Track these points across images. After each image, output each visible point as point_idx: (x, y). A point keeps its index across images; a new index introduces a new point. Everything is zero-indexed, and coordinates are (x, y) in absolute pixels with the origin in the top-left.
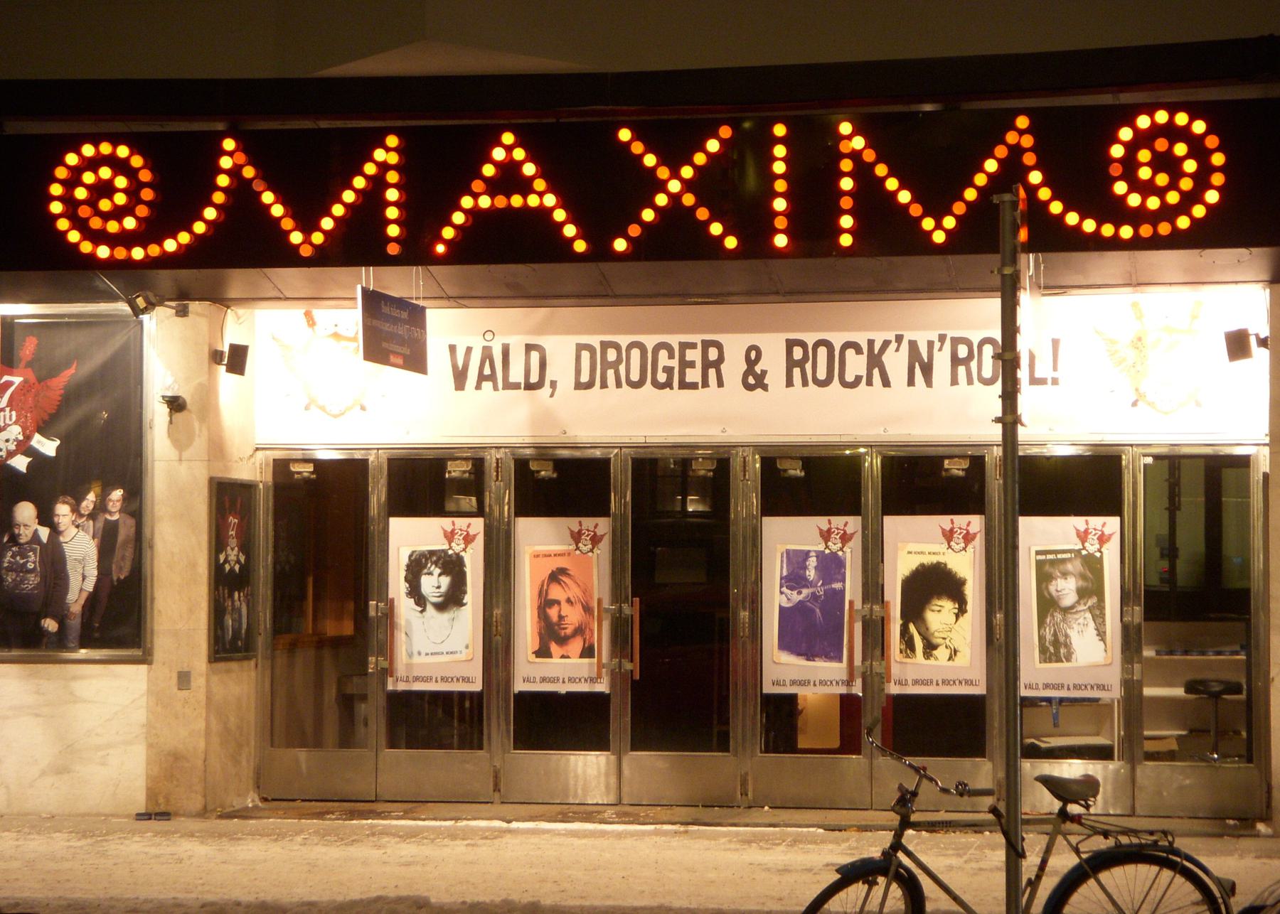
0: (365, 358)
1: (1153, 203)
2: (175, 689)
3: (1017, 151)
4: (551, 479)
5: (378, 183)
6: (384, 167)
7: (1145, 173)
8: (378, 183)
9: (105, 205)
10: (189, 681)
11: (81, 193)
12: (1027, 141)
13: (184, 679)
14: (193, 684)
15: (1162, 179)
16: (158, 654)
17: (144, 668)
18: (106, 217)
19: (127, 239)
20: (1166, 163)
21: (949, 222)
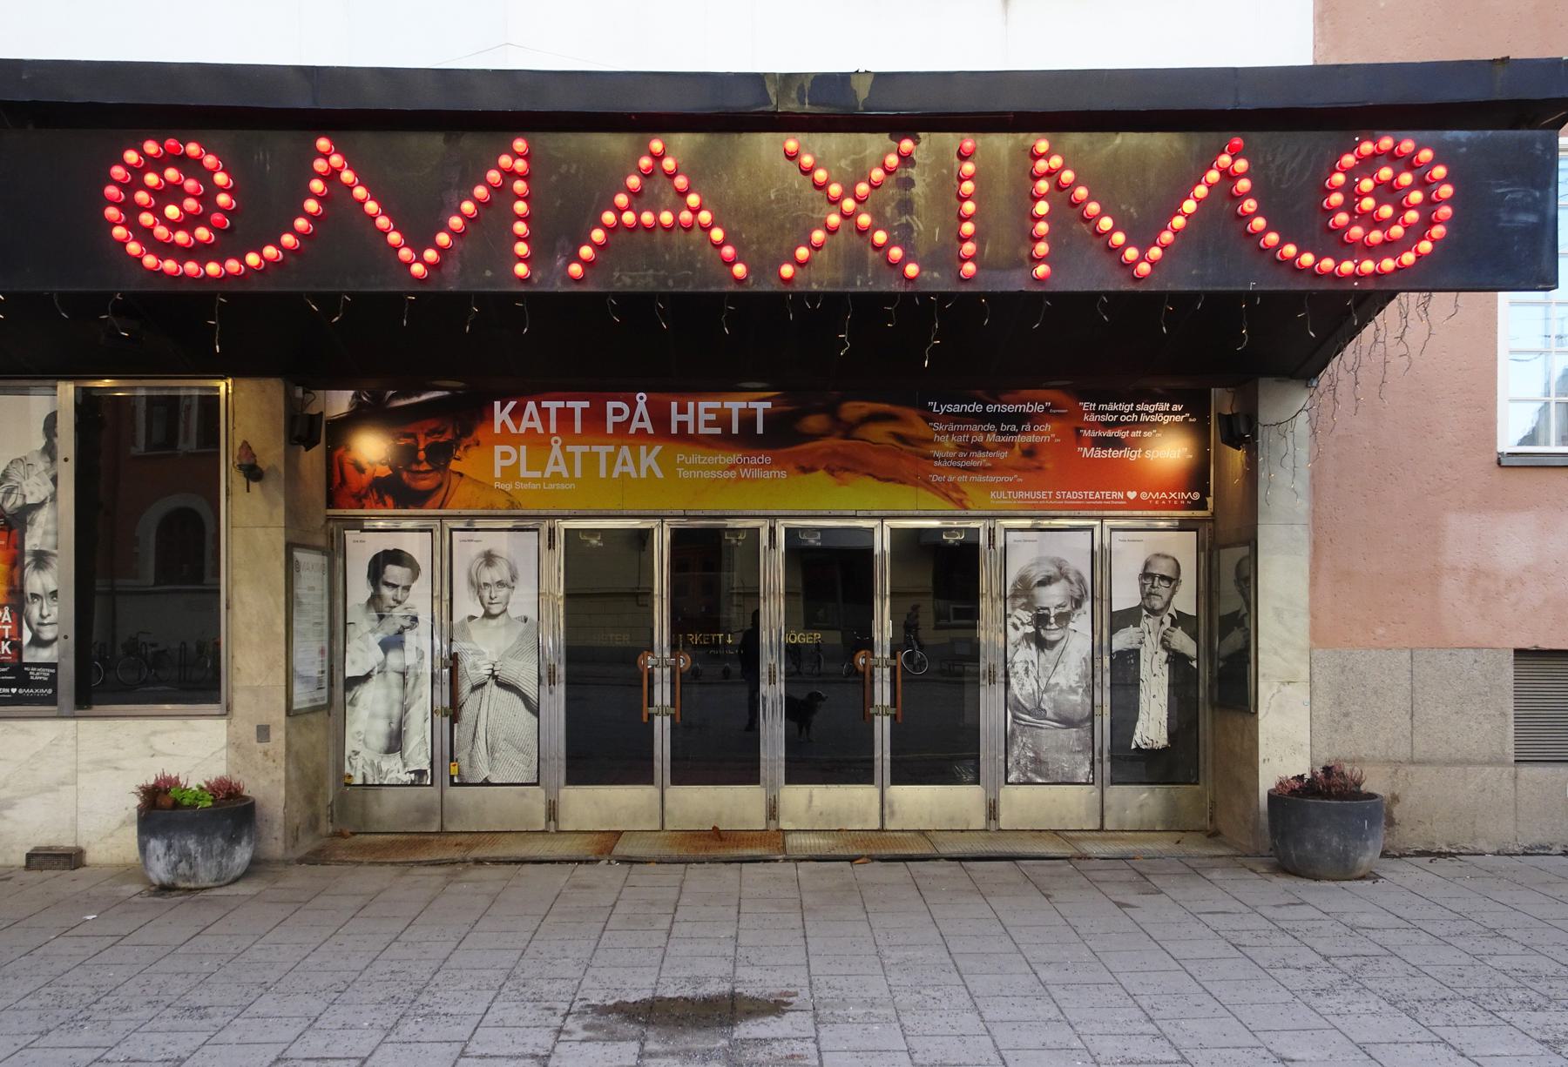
0: (1547, 281)
1: (1376, 236)
2: (254, 742)
3: (332, 176)
4: (598, 548)
5: (502, 193)
6: (509, 174)
7: (1368, 203)
8: (502, 193)
9: (172, 211)
10: (268, 735)
11: (142, 197)
12: (336, 160)
13: (263, 732)
14: (272, 737)
15: (1387, 211)
16: (238, 709)
17: (223, 722)
18: (173, 226)
19: (199, 252)
20: (1387, 191)
21: (1155, 252)
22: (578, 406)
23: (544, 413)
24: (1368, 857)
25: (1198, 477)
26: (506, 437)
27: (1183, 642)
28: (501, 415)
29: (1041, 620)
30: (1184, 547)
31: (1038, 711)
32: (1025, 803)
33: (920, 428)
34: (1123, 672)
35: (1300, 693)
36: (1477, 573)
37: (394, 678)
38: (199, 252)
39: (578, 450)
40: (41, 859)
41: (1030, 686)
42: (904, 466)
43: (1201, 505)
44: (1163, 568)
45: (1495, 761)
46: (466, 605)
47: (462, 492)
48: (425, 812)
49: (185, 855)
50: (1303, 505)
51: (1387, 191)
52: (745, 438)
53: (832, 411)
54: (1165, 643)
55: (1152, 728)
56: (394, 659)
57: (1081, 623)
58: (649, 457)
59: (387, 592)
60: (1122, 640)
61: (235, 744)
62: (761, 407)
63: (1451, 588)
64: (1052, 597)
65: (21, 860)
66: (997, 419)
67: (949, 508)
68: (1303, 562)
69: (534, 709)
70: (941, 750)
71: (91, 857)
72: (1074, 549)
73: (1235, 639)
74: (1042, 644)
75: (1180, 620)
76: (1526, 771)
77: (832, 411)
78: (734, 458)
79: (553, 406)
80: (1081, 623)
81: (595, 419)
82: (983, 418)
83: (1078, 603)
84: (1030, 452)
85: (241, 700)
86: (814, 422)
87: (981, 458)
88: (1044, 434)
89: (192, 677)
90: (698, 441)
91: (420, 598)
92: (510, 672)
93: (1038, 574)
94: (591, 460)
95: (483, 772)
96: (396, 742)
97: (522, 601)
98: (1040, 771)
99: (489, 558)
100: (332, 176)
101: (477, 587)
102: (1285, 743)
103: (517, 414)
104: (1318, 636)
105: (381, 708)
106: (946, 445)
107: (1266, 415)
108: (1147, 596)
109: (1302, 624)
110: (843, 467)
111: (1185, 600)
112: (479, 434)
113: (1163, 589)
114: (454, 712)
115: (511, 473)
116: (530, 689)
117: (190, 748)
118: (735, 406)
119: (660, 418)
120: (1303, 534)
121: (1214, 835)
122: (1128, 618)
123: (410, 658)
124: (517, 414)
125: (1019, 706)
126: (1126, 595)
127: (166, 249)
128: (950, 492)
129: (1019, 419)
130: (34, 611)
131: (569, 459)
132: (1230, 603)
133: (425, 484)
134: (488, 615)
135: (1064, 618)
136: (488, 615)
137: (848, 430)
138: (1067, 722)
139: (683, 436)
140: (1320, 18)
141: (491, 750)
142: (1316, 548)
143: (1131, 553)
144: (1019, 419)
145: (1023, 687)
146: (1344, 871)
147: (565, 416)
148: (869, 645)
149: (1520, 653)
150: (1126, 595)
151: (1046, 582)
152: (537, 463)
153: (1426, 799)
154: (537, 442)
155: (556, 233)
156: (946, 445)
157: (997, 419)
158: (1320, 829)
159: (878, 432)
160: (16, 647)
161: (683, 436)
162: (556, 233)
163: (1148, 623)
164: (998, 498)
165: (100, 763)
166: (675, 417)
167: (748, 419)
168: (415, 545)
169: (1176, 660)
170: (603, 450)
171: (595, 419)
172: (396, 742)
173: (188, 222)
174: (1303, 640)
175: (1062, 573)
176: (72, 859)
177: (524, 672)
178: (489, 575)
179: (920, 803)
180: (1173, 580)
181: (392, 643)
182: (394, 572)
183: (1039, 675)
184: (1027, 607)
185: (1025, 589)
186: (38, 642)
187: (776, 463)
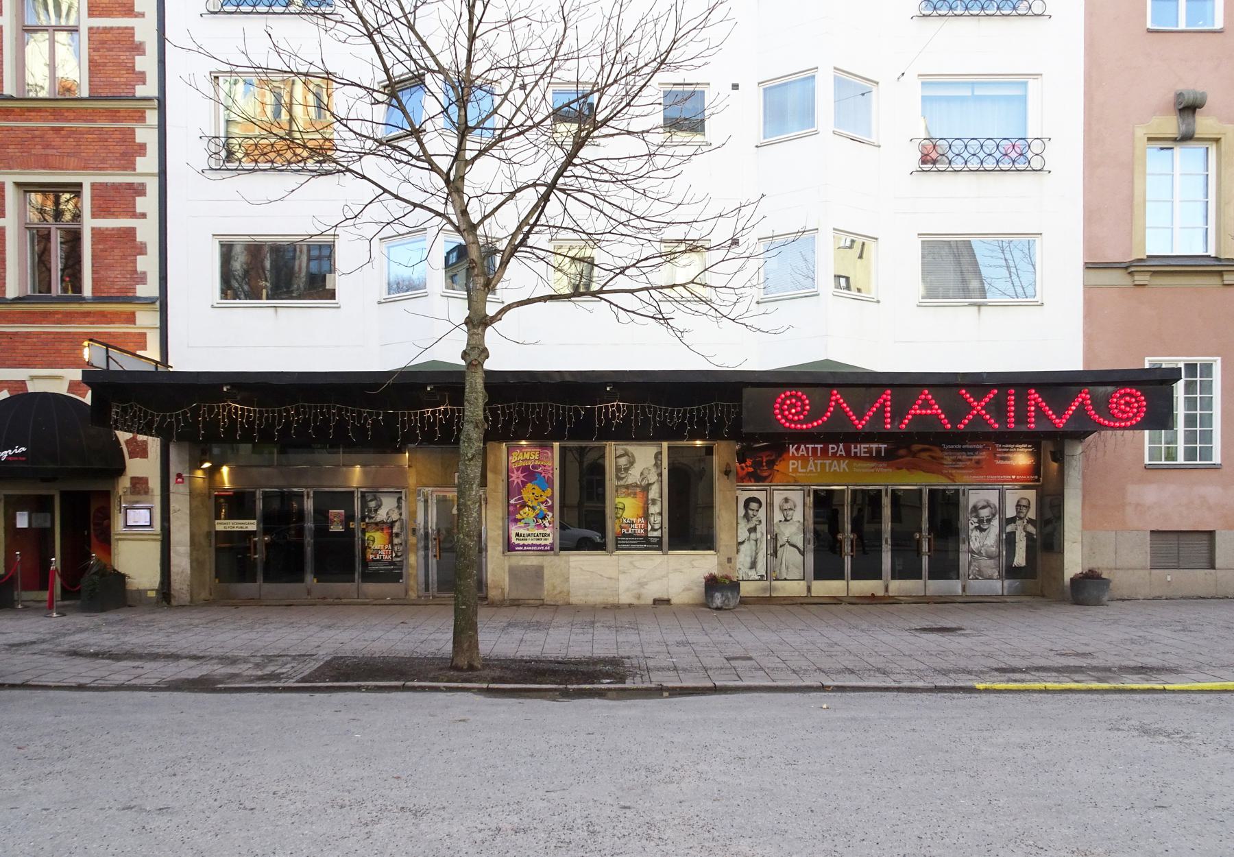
6: (886, 400)
8: (884, 406)
18: (794, 415)
19: (799, 421)
20: (1127, 404)
22: (819, 446)
23: (807, 449)
24: (1105, 598)
25: (1036, 469)
26: (794, 457)
27: (1031, 529)
28: (792, 450)
29: (981, 521)
30: (1031, 495)
31: (980, 553)
32: (978, 587)
33: (938, 453)
34: (1009, 541)
35: (1078, 547)
36: (1138, 505)
37: (753, 543)
38: (799, 421)
39: (819, 462)
40: (657, 602)
41: (977, 545)
42: (934, 466)
43: (1038, 480)
44: (1024, 503)
45: (1143, 568)
46: (778, 516)
47: (778, 477)
48: (764, 590)
49: (728, 598)
50: (1080, 483)
51: (1127, 404)
52: (877, 458)
53: (908, 448)
54: (1024, 529)
55: (1020, 559)
56: (753, 536)
57: (995, 522)
58: (844, 464)
59: (751, 512)
60: (1009, 529)
61: (720, 564)
62: (883, 446)
63: (1129, 510)
64: (985, 513)
65: (650, 601)
66: (966, 450)
67: (949, 482)
68: (1079, 501)
69: (803, 553)
70: (946, 568)
71: (673, 601)
72: (993, 496)
73: (1049, 529)
74: (982, 530)
75: (1030, 521)
76: (1154, 571)
77: (908, 448)
78: (873, 464)
79: (810, 446)
80: (995, 522)
81: (825, 451)
82: (961, 450)
83: (994, 515)
84: (978, 462)
85: (722, 549)
86: (902, 452)
87: (961, 464)
88: (983, 455)
89: (706, 542)
90: (861, 458)
91: (762, 514)
92: (793, 541)
93: (980, 505)
94: (823, 465)
95: (784, 576)
96: (753, 565)
97: (798, 516)
98: (980, 575)
99: (786, 500)
100: (837, 400)
101: (782, 510)
102: (1074, 562)
103: (798, 449)
104: (1084, 527)
105: (749, 553)
106: (948, 459)
107: (1067, 452)
108: (1018, 512)
109: (1079, 523)
110: (912, 467)
111: (1032, 514)
112: (785, 456)
113: (1024, 510)
114: (775, 553)
115: (795, 470)
116: (801, 545)
117: (703, 564)
118: (874, 446)
119: (848, 451)
120: (1079, 492)
121: (1043, 596)
122: (1012, 520)
123: (759, 535)
124: (798, 449)
125: (973, 552)
126: (1010, 512)
127: (792, 421)
128: (950, 477)
129: (974, 450)
130: (652, 519)
131: (816, 465)
132: (1048, 514)
133: (765, 474)
134: (786, 520)
135: (989, 521)
136: (786, 520)
137: (914, 454)
138: (990, 557)
139: (856, 457)
140: (1085, 317)
141: (787, 568)
142: (1084, 496)
143: (1012, 498)
144: (974, 450)
145: (974, 545)
146: (1098, 603)
147: (814, 450)
148: (920, 531)
149: (1152, 532)
150: (1010, 512)
151: (984, 507)
152: (804, 466)
153: (1120, 581)
154: (805, 459)
155: (898, 415)
156: (948, 459)
157: (966, 450)
158: (1088, 590)
159: (925, 455)
160: (646, 531)
161: (856, 457)
162: (898, 415)
163: (1019, 522)
164: (966, 478)
165: (676, 570)
166: (853, 450)
167: (879, 451)
168: (761, 496)
169: (1029, 536)
170: (828, 462)
171: (825, 451)
172: (753, 565)
173: (797, 413)
174: (1079, 527)
175: (987, 505)
176: (668, 601)
177: (798, 540)
178: (787, 506)
179: (936, 587)
180: (1028, 507)
181: (753, 530)
182: (754, 505)
183: (982, 540)
184: (976, 517)
185: (975, 509)
186: (653, 529)
187: (888, 466)
